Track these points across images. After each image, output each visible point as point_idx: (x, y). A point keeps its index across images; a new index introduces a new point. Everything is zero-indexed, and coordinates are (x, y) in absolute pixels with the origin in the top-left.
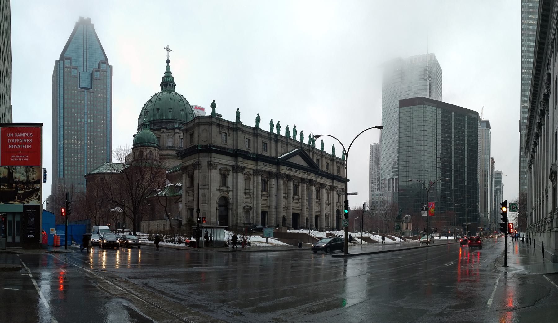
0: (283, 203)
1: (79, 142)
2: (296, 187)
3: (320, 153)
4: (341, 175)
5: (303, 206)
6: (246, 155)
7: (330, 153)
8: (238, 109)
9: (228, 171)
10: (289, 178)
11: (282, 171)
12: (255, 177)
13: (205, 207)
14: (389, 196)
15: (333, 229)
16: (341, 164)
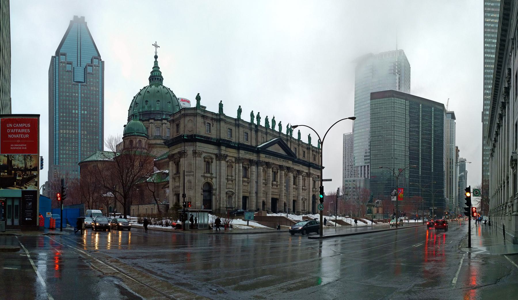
0: (262, 189)
1: (74, 132)
5: (281, 191)
6: (228, 144)
8: (221, 101)
9: (212, 159)
10: (268, 165)
12: (237, 165)
14: (361, 182)
15: (309, 213)
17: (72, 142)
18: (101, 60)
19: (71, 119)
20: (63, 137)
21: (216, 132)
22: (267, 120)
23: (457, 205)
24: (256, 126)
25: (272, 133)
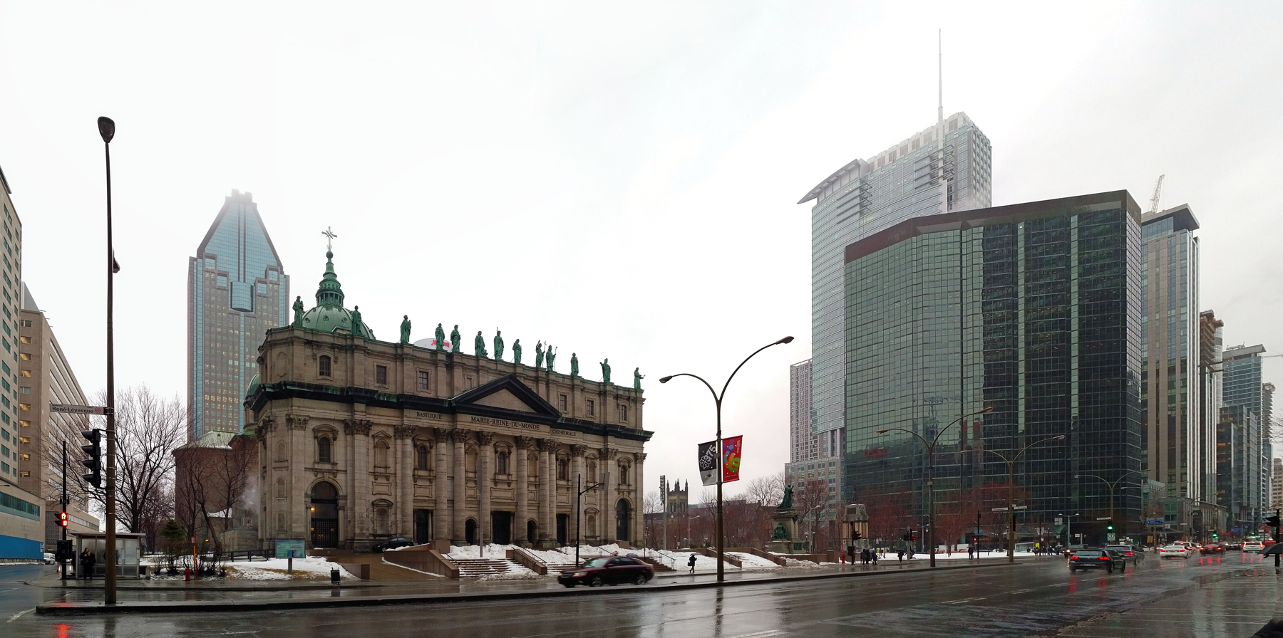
0: (466, 491)
1: (230, 400)
2: (503, 457)
4: (630, 424)
5: (520, 495)
6: (371, 399)
7: (599, 377)
10: (481, 438)
12: (399, 442)
15: (606, 542)
16: (629, 399)
17: (228, 419)
22: (479, 342)
23: (1212, 498)
24: (450, 356)
25: (493, 366)
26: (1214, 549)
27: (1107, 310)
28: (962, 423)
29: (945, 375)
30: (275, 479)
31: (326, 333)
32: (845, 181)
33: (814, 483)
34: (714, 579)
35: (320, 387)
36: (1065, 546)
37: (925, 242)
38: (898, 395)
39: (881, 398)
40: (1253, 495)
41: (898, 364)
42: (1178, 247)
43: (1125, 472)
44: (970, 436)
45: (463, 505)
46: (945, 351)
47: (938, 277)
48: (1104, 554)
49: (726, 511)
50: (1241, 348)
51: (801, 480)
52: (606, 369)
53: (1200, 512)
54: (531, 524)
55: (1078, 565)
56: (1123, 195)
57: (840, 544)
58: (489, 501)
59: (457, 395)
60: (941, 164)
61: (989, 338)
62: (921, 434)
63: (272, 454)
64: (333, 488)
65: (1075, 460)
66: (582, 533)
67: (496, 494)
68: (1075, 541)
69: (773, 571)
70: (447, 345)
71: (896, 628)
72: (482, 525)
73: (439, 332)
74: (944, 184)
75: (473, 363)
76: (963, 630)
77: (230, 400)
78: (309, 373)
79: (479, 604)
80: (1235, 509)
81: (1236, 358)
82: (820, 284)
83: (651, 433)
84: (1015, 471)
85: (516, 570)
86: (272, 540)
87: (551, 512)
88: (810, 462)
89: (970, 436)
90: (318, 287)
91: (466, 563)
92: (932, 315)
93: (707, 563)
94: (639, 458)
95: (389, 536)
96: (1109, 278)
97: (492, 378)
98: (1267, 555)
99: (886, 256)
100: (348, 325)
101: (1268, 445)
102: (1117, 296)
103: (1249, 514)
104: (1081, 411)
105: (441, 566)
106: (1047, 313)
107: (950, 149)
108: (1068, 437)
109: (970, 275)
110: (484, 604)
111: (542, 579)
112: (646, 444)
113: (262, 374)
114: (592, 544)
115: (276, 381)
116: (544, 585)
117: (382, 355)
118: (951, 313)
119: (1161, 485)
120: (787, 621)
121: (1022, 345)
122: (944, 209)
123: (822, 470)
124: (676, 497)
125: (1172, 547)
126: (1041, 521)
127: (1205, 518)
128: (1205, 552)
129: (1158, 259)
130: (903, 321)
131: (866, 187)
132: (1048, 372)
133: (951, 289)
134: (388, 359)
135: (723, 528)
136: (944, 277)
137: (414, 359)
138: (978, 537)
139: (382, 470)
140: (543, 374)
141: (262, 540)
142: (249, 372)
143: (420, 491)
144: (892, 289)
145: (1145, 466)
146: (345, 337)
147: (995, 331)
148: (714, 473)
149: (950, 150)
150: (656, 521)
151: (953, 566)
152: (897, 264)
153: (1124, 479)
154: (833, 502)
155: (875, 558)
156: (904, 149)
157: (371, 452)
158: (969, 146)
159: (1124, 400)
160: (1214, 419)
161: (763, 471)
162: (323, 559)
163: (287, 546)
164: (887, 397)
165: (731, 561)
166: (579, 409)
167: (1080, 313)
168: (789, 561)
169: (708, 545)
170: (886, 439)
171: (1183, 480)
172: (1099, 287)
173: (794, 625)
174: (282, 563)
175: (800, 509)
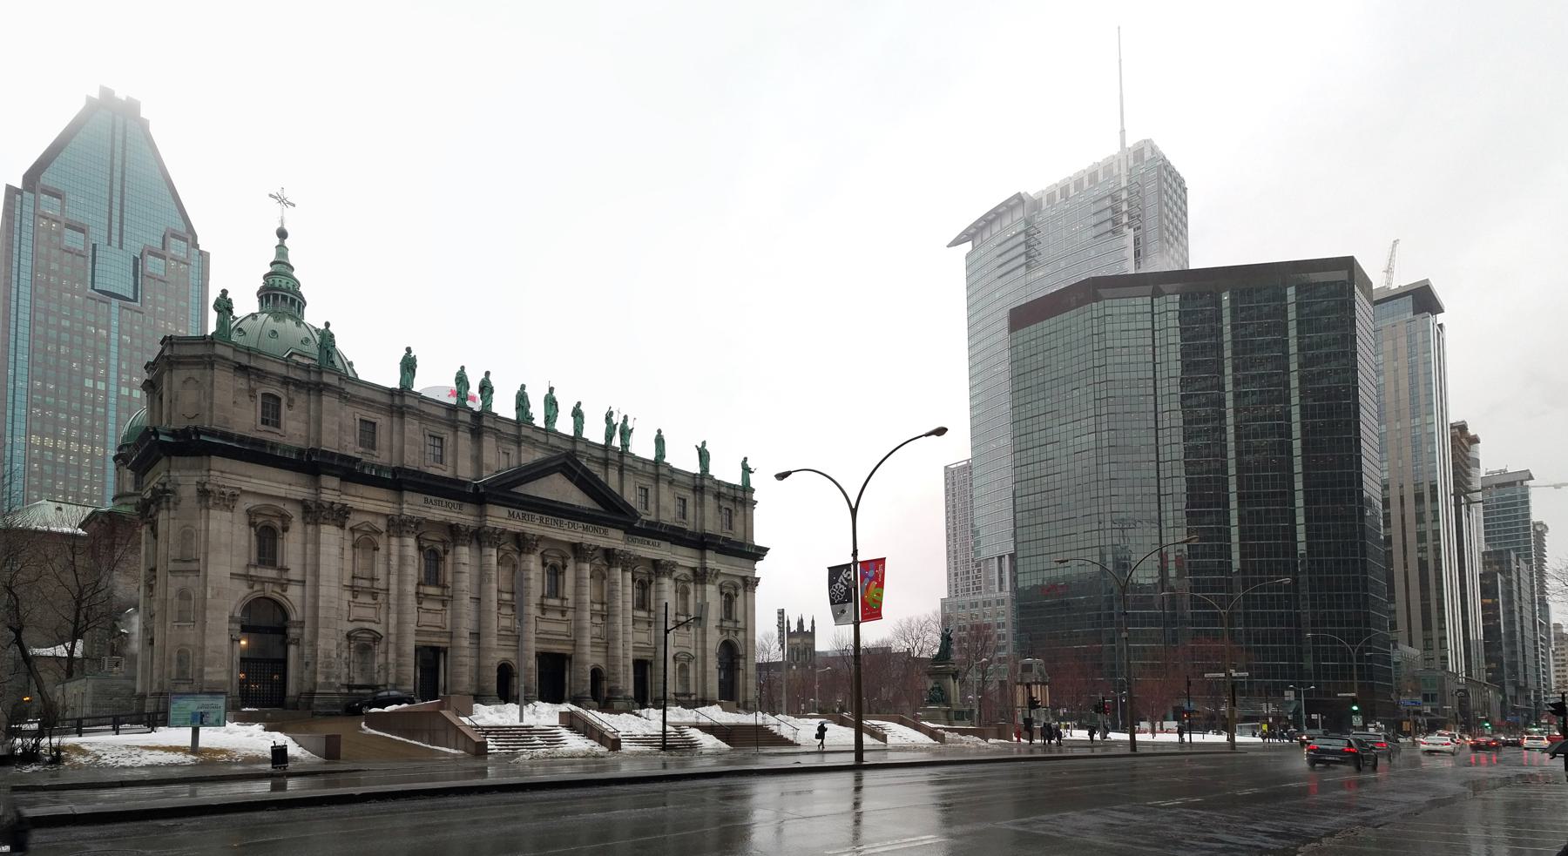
0: (497, 621)
1: (87, 449)
2: (555, 573)
3: (650, 469)
4: (737, 536)
5: (579, 629)
6: (351, 472)
9: (286, 518)
10: (522, 543)
11: (490, 523)
12: (394, 541)
13: (188, 631)
14: (996, 605)
15: (705, 702)
16: (734, 499)
18: (196, 246)
19: (75, 405)
20: (41, 460)
21: (302, 426)
22: (522, 401)
23: (1480, 674)
24: (478, 416)
25: (542, 438)
26: (1487, 743)
27: (1336, 414)
28: (1161, 555)
29: (1138, 490)
30: (172, 591)
31: (275, 358)
32: (1007, 222)
33: (977, 628)
34: (850, 759)
35: (262, 443)
36: (1300, 730)
37: (1108, 311)
38: (1080, 513)
39: (1059, 517)
40: (1531, 672)
41: (1078, 471)
42: (1419, 335)
43: (1369, 633)
44: (1173, 573)
45: (494, 642)
46: (1136, 457)
47: (1125, 359)
48: (1350, 744)
49: (865, 663)
50: (1503, 472)
51: (962, 623)
52: (703, 455)
53: (1465, 691)
54: (596, 674)
55: (1317, 758)
56: (1348, 264)
57: (1014, 714)
58: (533, 636)
59: (487, 476)
60: (1125, 207)
61: (1191, 443)
62: (1110, 567)
63: (169, 546)
64: (281, 609)
65: (1306, 612)
66: (671, 689)
67: (544, 626)
68: (1312, 725)
69: (928, 749)
70: (473, 399)
71: (1091, 838)
72: (523, 673)
73: (461, 379)
74: (1130, 234)
75: (512, 430)
76: (1177, 843)
77: (87, 449)
78: (245, 420)
79: (520, 796)
80: (1510, 690)
81: (1498, 486)
82: (979, 358)
83: (766, 550)
84: (1231, 624)
85: (575, 743)
86: (163, 696)
87: (626, 656)
88: (972, 598)
89: (1173, 573)
90: (261, 283)
91: (498, 731)
92: (1119, 409)
93: (841, 736)
94: (751, 583)
95: (375, 687)
96: (1336, 372)
97: (539, 455)
98: (1554, 756)
99: (1060, 326)
100: (313, 349)
101: (1544, 605)
102: (1347, 396)
103: (1528, 698)
104: (1309, 546)
105: (456, 735)
106: (1261, 414)
107: (1135, 188)
108: (1295, 581)
109: (1164, 358)
110: (528, 796)
111: (613, 757)
112: (759, 565)
113: (151, 409)
114: (686, 706)
115: (179, 424)
116: (617, 766)
117: (367, 403)
118: (1142, 408)
119: (1415, 652)
120: (948, 822)
121: (1231, 454)
122: (1130, 268)
123: (988, 610)
124: (799, 639)
125: (1434, 738)
126: (1268, 693)
127: (1473, 702)
128: (1476, 747)
129: (1395, 350)
130: (1084, 415)
131: (1032, 231)
132: (1264, 494)
133: (1141, 375)
134: (379, 410)
135: (862, 686)
136: (1133, 359)
137: (422, 416)
138: (1189, 713)
139: (366, 584)
140: (616, 456)
141: (143, 697)
142: (125, 405)
143: (427, 618)
144: (1068, 371)
145: (1393, 626)
146: (307, 368)
147: (1199, 434)
148: (850, 607)
149: (1136, 189)
150: (774, 674)
151: (1160, 752)
152: (1074, 337)
153: (1369, 642)
154: (1003, 654)
155: (1059, 736)
156: (1078, 184)
157: (348, 554)
158: (1160, 184)
159: (1363, 536)
160: (1476, 567)
161: (912, 610)
162: (257, 728)
163: (192, 705)
164: (1066, 515)
165: (874, 733)
166: (666, 508)
167: (1302, 416)
168: (948, 735)
169: (843, 710)
170: (1067, 571)
171: (1443, 647)
172: (1325, 384)
173: (957, 830)
174: (182, 736)
175: (962, 663)
